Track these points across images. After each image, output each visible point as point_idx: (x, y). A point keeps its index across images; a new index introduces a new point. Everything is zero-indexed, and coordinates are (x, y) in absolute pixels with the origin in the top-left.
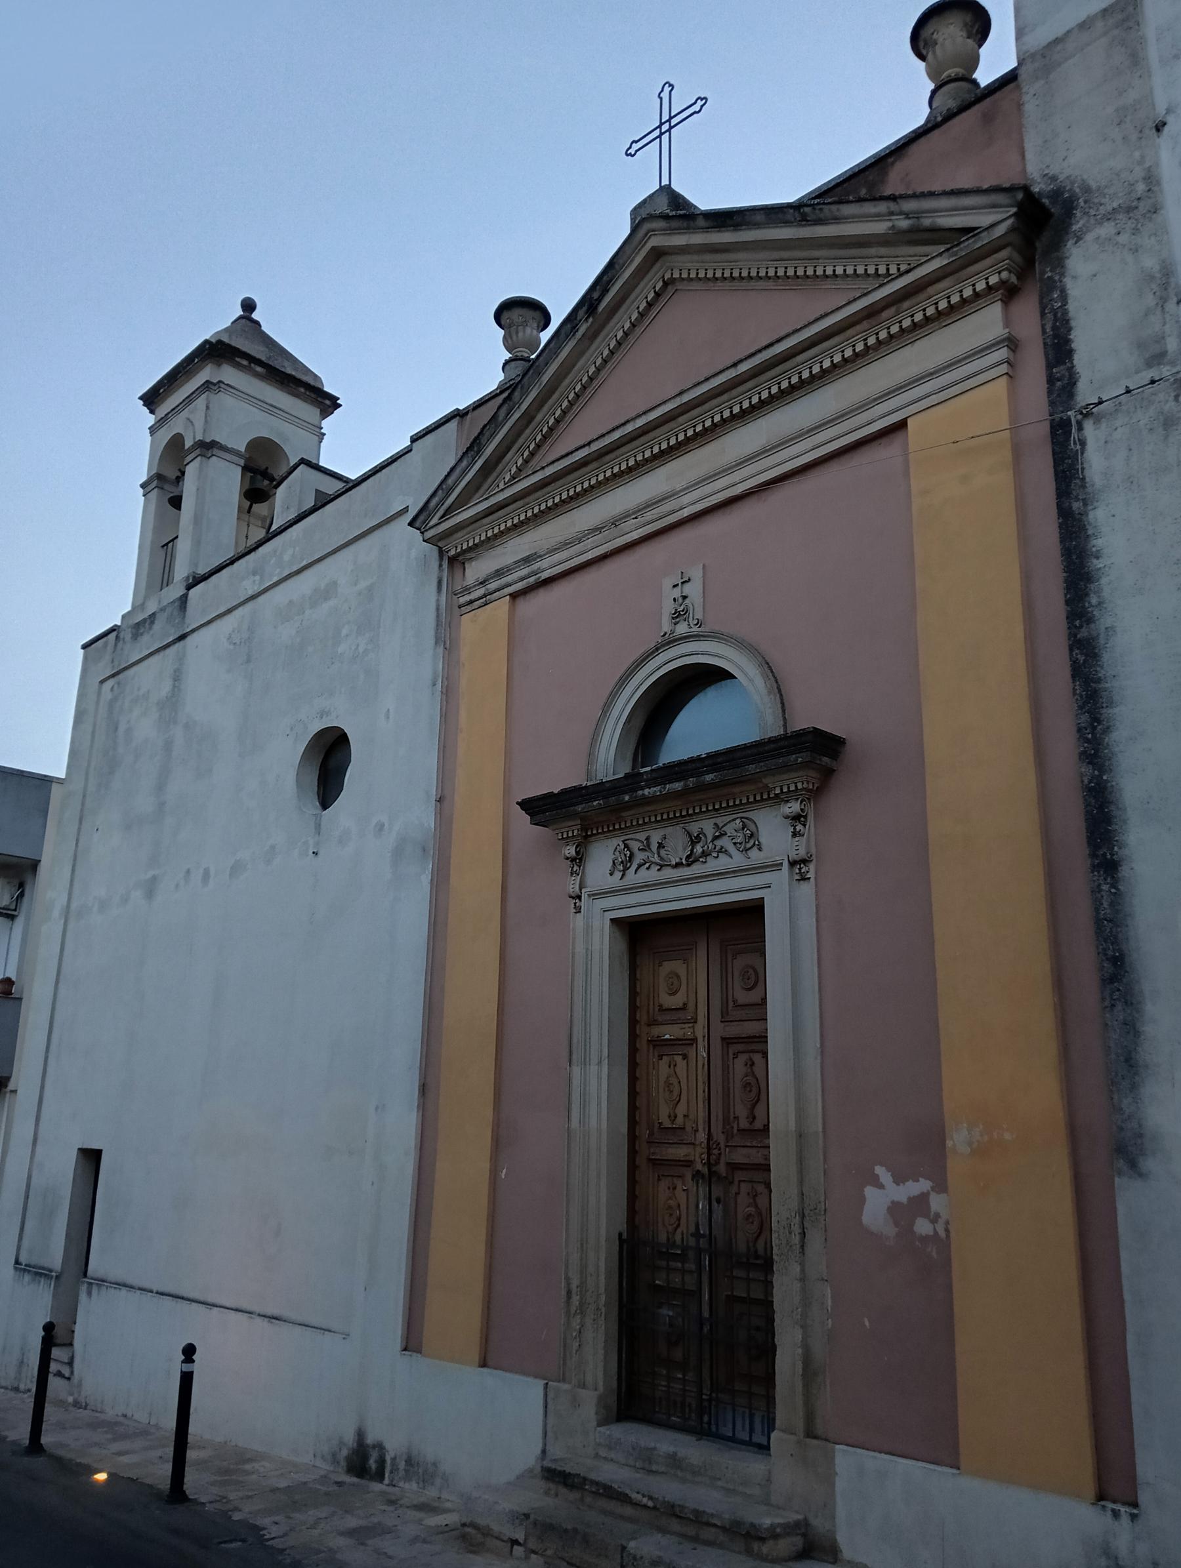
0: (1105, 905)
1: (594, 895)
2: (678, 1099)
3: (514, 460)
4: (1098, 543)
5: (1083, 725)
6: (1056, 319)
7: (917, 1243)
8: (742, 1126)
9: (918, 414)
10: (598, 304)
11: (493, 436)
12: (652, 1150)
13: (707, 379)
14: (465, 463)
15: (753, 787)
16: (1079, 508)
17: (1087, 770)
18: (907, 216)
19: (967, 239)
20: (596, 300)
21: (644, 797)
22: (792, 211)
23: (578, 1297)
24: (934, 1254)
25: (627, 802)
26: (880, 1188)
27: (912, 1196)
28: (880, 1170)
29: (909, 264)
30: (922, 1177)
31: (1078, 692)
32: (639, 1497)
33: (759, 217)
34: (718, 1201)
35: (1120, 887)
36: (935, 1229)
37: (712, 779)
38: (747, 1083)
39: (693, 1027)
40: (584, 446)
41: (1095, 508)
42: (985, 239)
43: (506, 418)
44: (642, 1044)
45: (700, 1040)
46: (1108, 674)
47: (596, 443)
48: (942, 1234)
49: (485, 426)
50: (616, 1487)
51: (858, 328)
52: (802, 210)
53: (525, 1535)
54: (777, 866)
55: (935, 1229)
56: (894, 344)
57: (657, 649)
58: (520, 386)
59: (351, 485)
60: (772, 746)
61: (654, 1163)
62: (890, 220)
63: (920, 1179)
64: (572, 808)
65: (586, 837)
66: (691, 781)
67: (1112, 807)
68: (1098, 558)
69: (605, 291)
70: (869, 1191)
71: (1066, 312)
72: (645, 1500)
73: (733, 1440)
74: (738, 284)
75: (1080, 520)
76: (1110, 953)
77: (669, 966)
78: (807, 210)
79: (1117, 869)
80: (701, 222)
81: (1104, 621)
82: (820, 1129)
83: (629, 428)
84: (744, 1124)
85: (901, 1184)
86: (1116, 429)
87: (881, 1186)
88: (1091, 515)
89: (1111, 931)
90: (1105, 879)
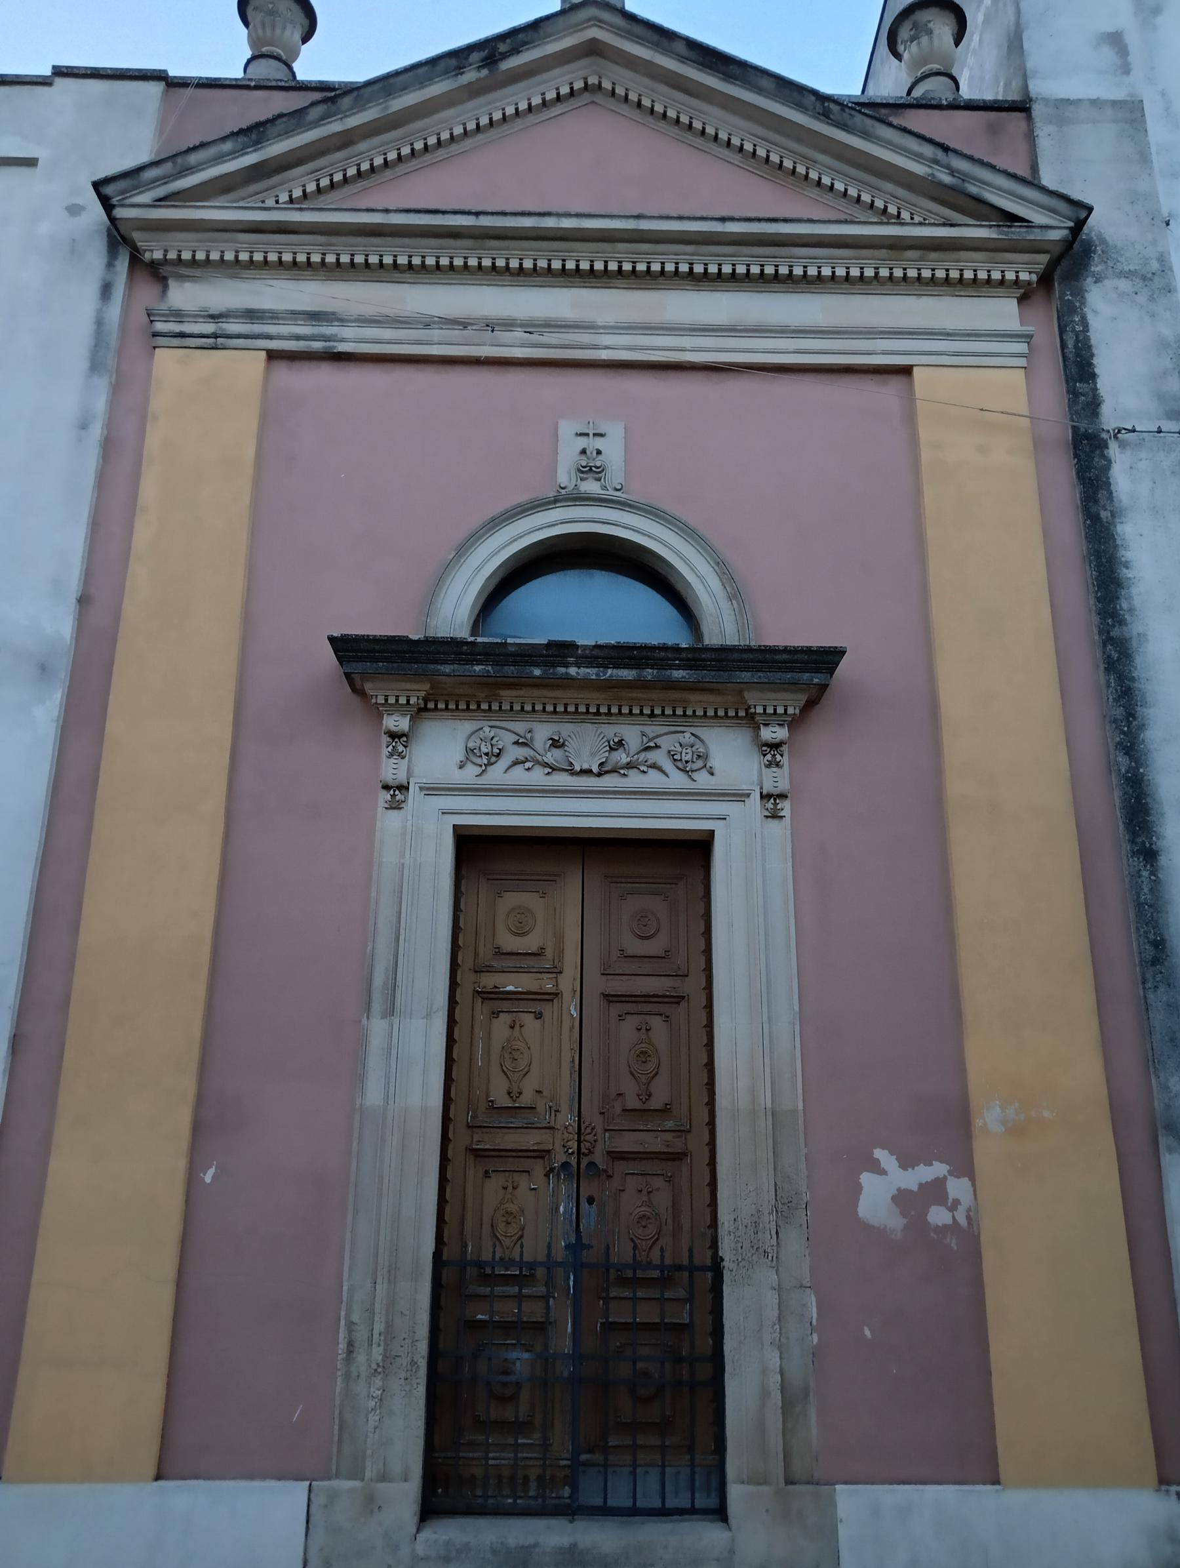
0: (1146, 890)
1: (431, 790)
3: (301, 181)
4: (1127, 555)
5: (1119, 717)
6: (1077, 341)
7: (932, 1235)
8: (630, 1106)
9: (926, 368)
10: (501, 60)
11: (287, 133)
13: (680, 218)
14: (228, 146)
15: (718, 699)
16: (1107, 518)
17: (1123, 760)
18: (952, 172)
19: (1021, 226)
20: (501, 54)
21: (568, 677)
22: (813, 98)
24: (954, 1245)
25: (538, 677)
26: (881, 1174)
28: (880, 1154)
29: (925, 219)
30: (936, 1160)
31: (1113, 685)
33: (766, 83)
34: (591, 1201)
35: (1159, 875)
36: (953, 1216)
37: (683, 677)
38: (642, 1052)
39: (556, 978)
40: (469, 213)
41: (1122, 523)
42: (1036, 235)
43: (316, 123)
44: (464, 995)
45: (567, 995)
46: (1141, 676)
47: (490, 218)
48: (963, 1221)
49: (281, 116)
51: (876, 253)
52: (826, 104)
54: (741, 797)
55: (953, 1216)
56: (903, 287)
57: (556, 501)
58: (355, 93)
59: (293, 84)
60: (785, 656)
61: (478, 1154)
62: (931, 167)
63: (934, 1162)
64: (432, 666)
65: (425, 709)
66: (649, 674)
67: (1149, 800)
68: (1127, 568)
69: (515, 51)
70: (866, 1178)
71: (1088, 339)
73: (634, 1512)
74: (690, 137)
75: (1108, 529)
76: (1152, 936)
77: (511, 900)
78: (832, 106)
79: (1156, 858)
80: (681, 48)
81: (1135, 628)
83: (550, 223)
84: (633, 1102)
85: (910, 1170)
86: (1141, 460)
87: (883, 1172)
88: (1119, 528)
89: (1152, 916)
90: (1145, 866)
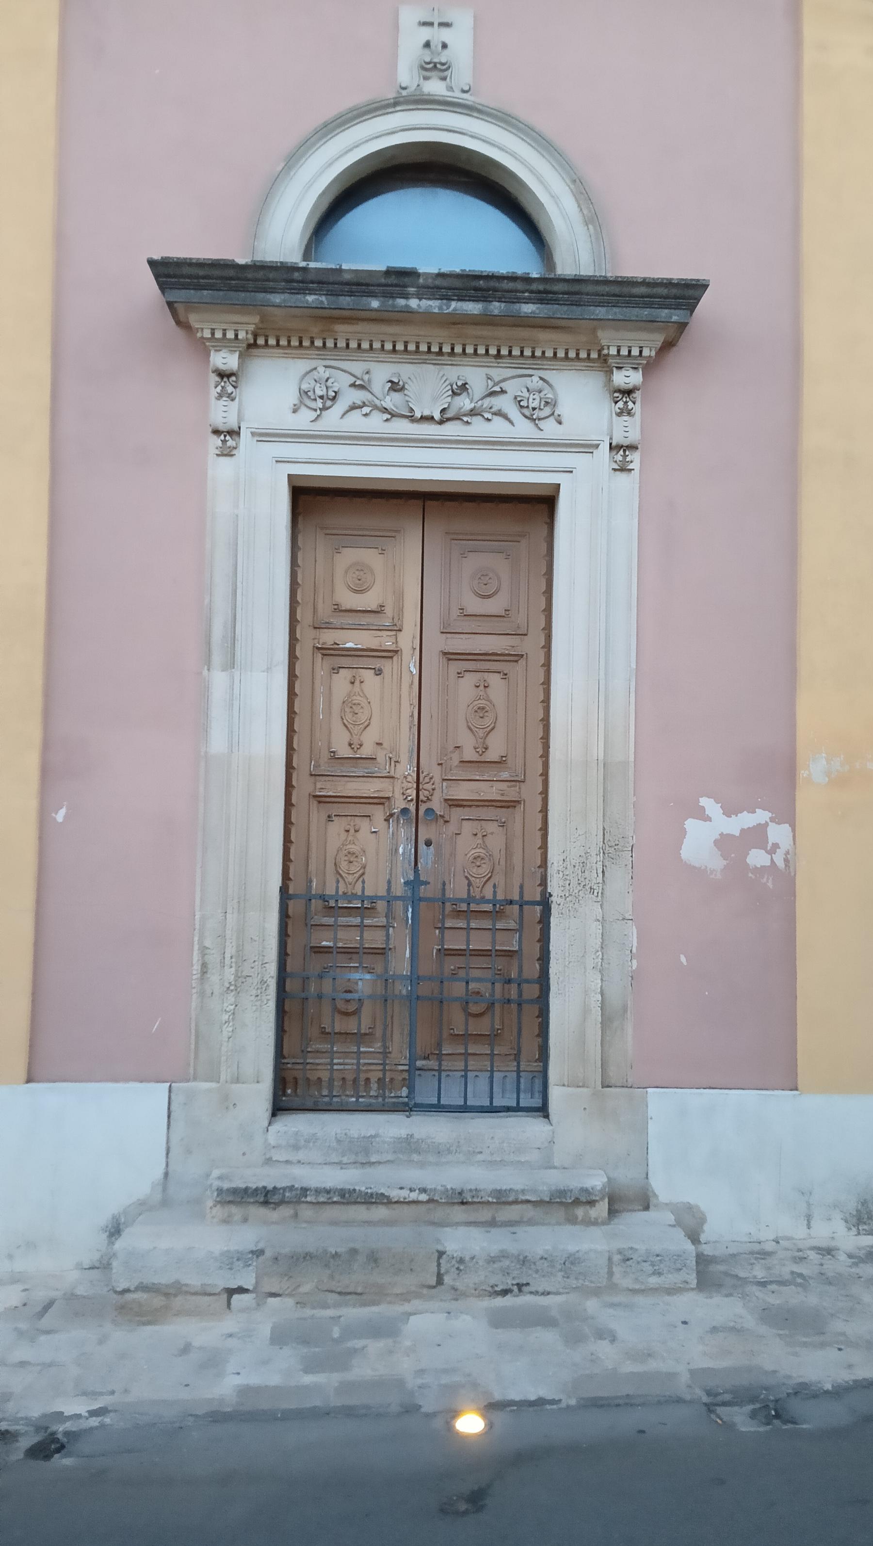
2: (366, 723)
12: (319, 785)
21: (409, 311)
23: (233, 969)
24: (770, 885)
25: (376, 310)
27: (746, 827)
28: (704, 801)
32: (404, 1193)
34: (428, 843)
36: (772, 859)
44: (304, 651)
50: (363, 1189)
53: (256, 1278)
54: (589, 448)
63: (757, 810)
66: (496, 308)
70: (691, 824)
72: (414, 1196)
73: (465, 1108)
77: (350, 556)
82: (632, 759)
84: (469, 754)
